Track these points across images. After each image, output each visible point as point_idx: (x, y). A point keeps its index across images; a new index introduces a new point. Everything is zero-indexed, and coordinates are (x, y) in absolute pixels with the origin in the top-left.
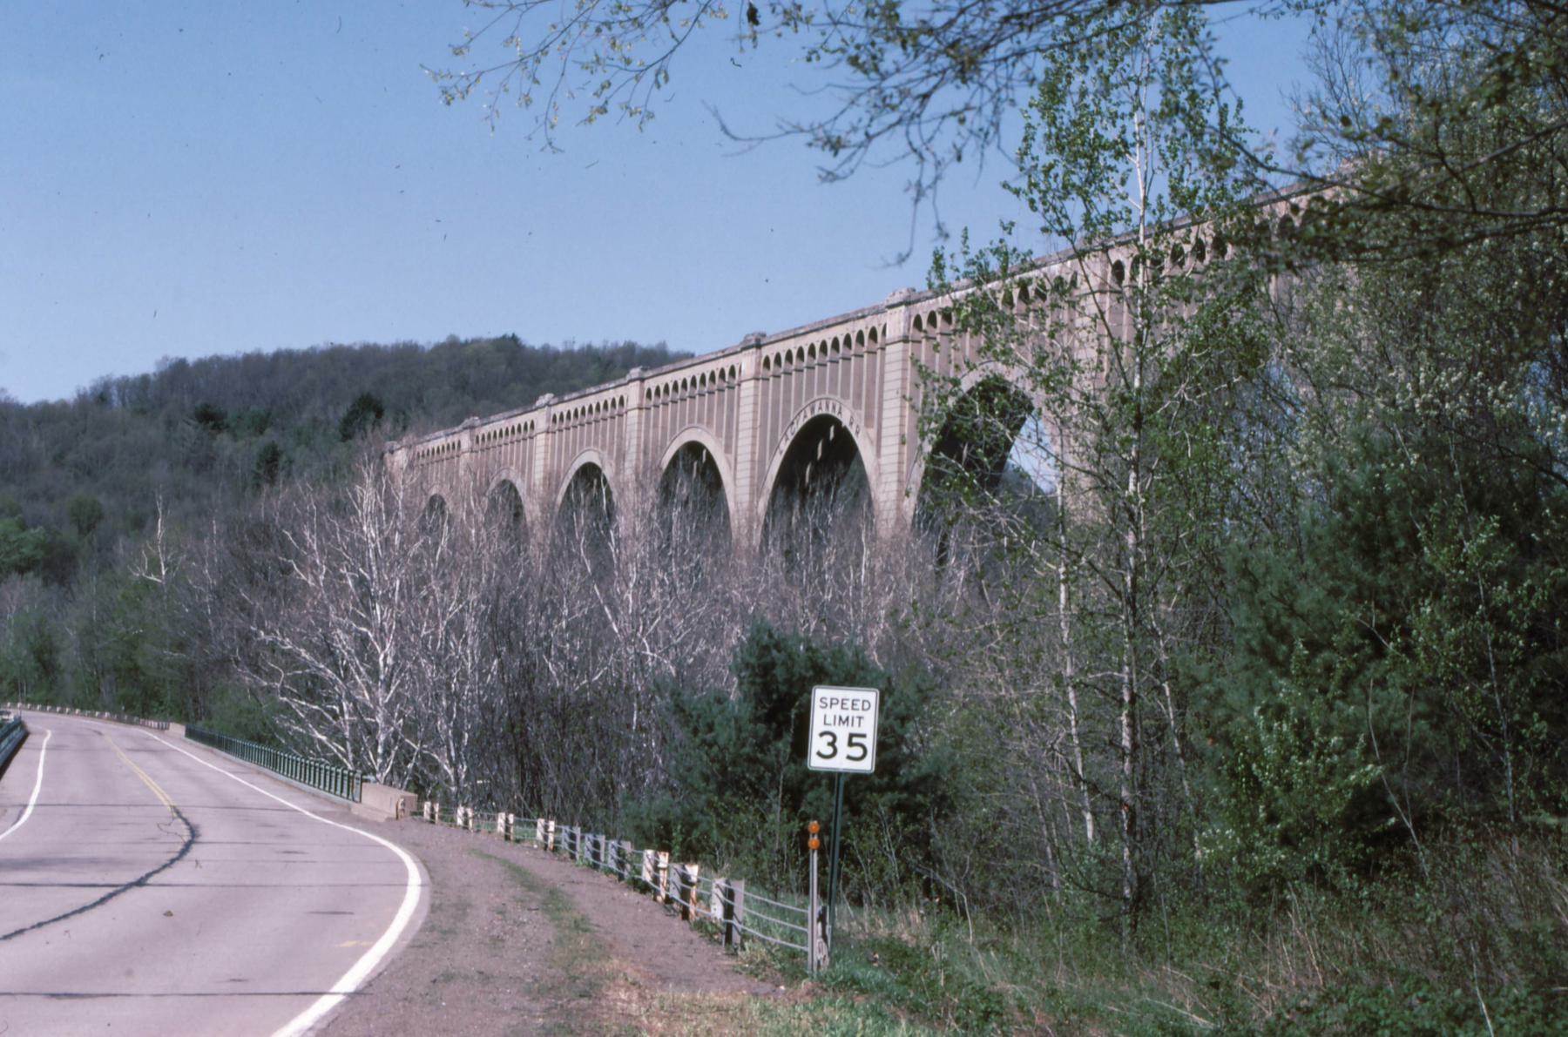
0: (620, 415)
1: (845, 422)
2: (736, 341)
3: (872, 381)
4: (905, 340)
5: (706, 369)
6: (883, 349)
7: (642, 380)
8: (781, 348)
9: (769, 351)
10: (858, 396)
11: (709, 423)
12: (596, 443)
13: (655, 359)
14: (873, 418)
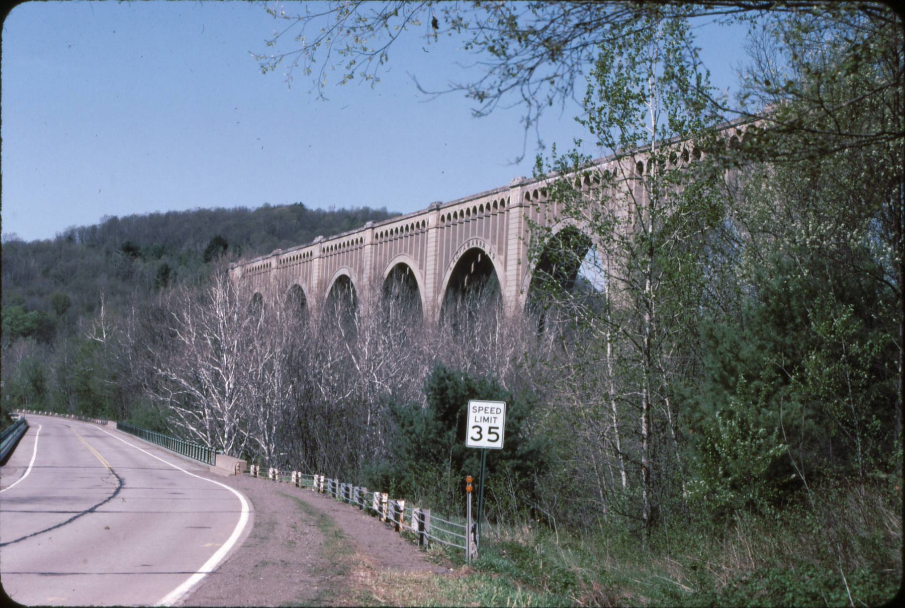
0: (361, 248)
1: (487, 252)
2: (425, 206)
3: (502, 229)
4: (521, 206)
5: (409, 222)
6: (508, 211)
7: (373, 228)
8: (451, 210)
9: (445, 212)
10: (494, 237)
11: (411, 253)
12: (347, 264)
13: (380, 217)
14: (502, 249)
